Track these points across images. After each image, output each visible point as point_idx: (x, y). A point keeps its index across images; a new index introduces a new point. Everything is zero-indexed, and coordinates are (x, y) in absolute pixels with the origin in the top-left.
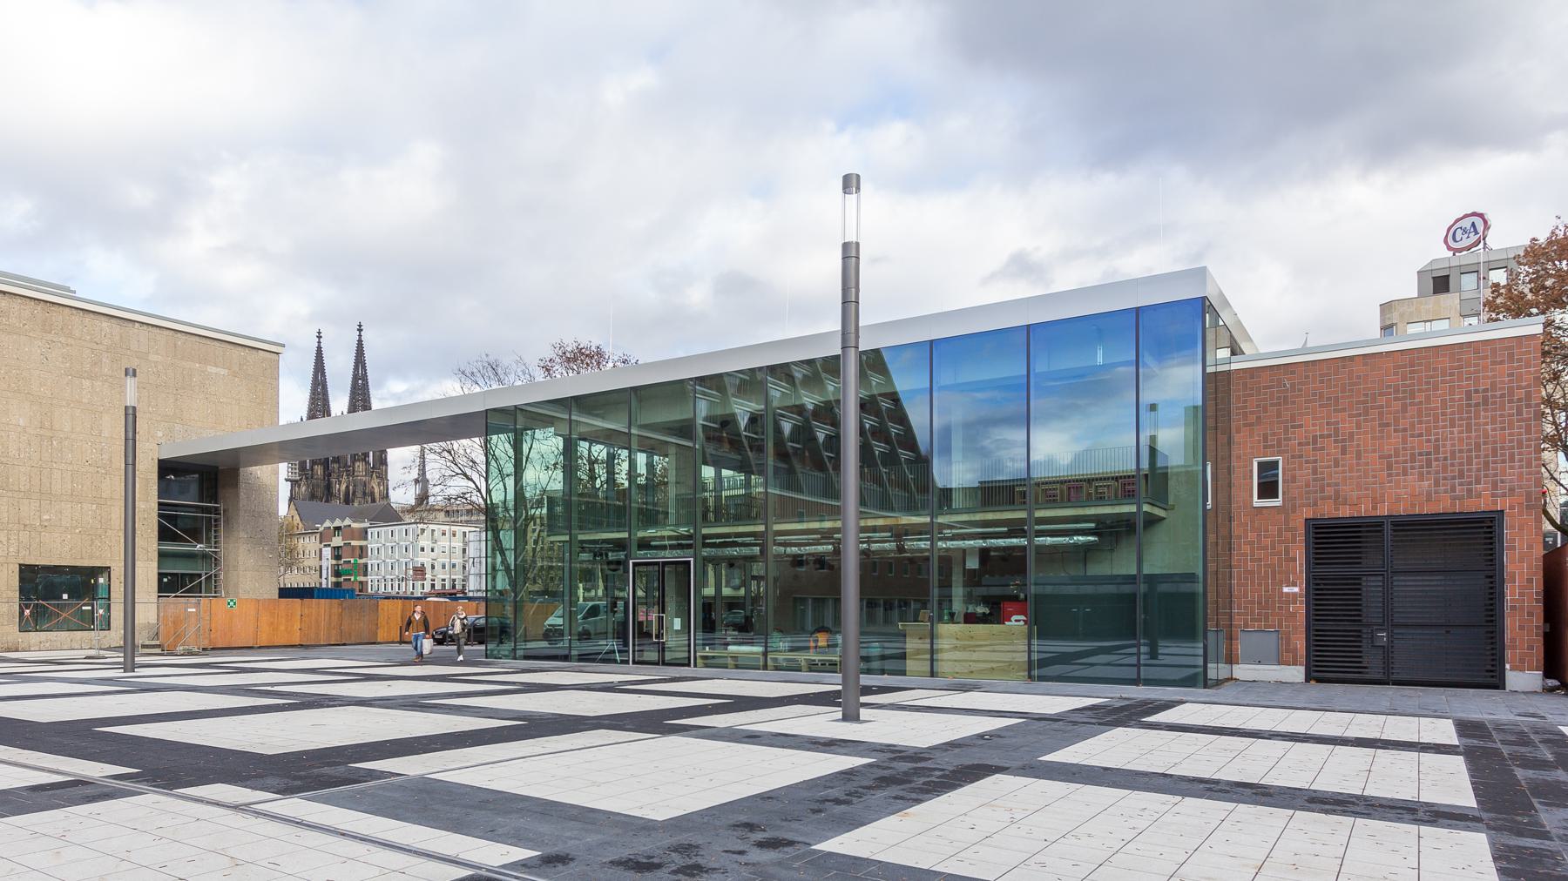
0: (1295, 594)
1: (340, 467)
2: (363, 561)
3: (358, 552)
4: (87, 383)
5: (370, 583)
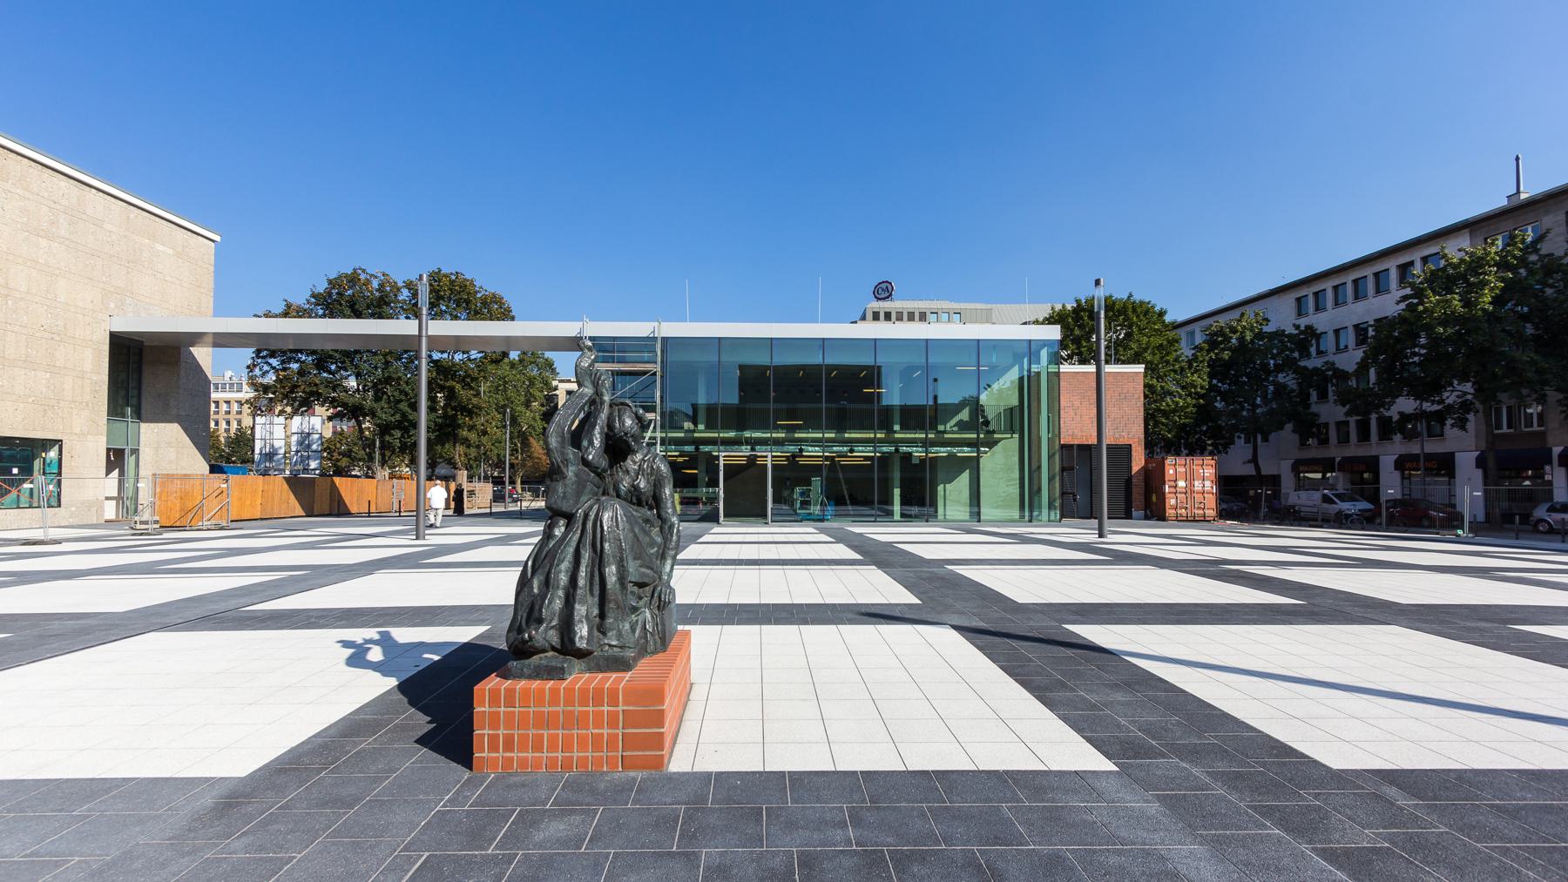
0: (1478, 496)
4: (43, 243)
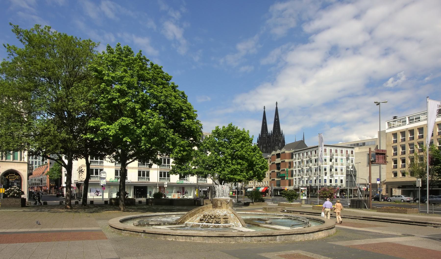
1: (270, 148)
2: (291, 169)
3: (288, 165)
5: (294, 180)
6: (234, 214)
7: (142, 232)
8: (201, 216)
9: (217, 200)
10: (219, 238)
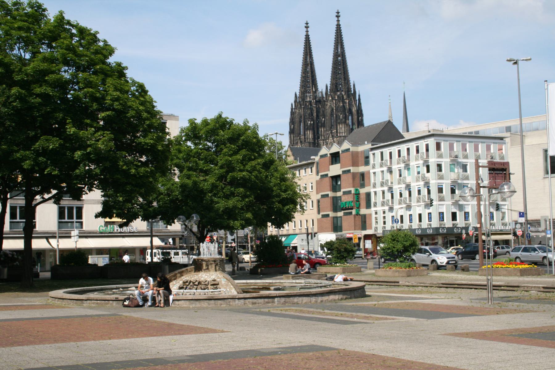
5: (374, 216)
6: (226, 279)
7: (114, 299)
8: (179, 283)
9: (202, 260)
10: (208, 301)
